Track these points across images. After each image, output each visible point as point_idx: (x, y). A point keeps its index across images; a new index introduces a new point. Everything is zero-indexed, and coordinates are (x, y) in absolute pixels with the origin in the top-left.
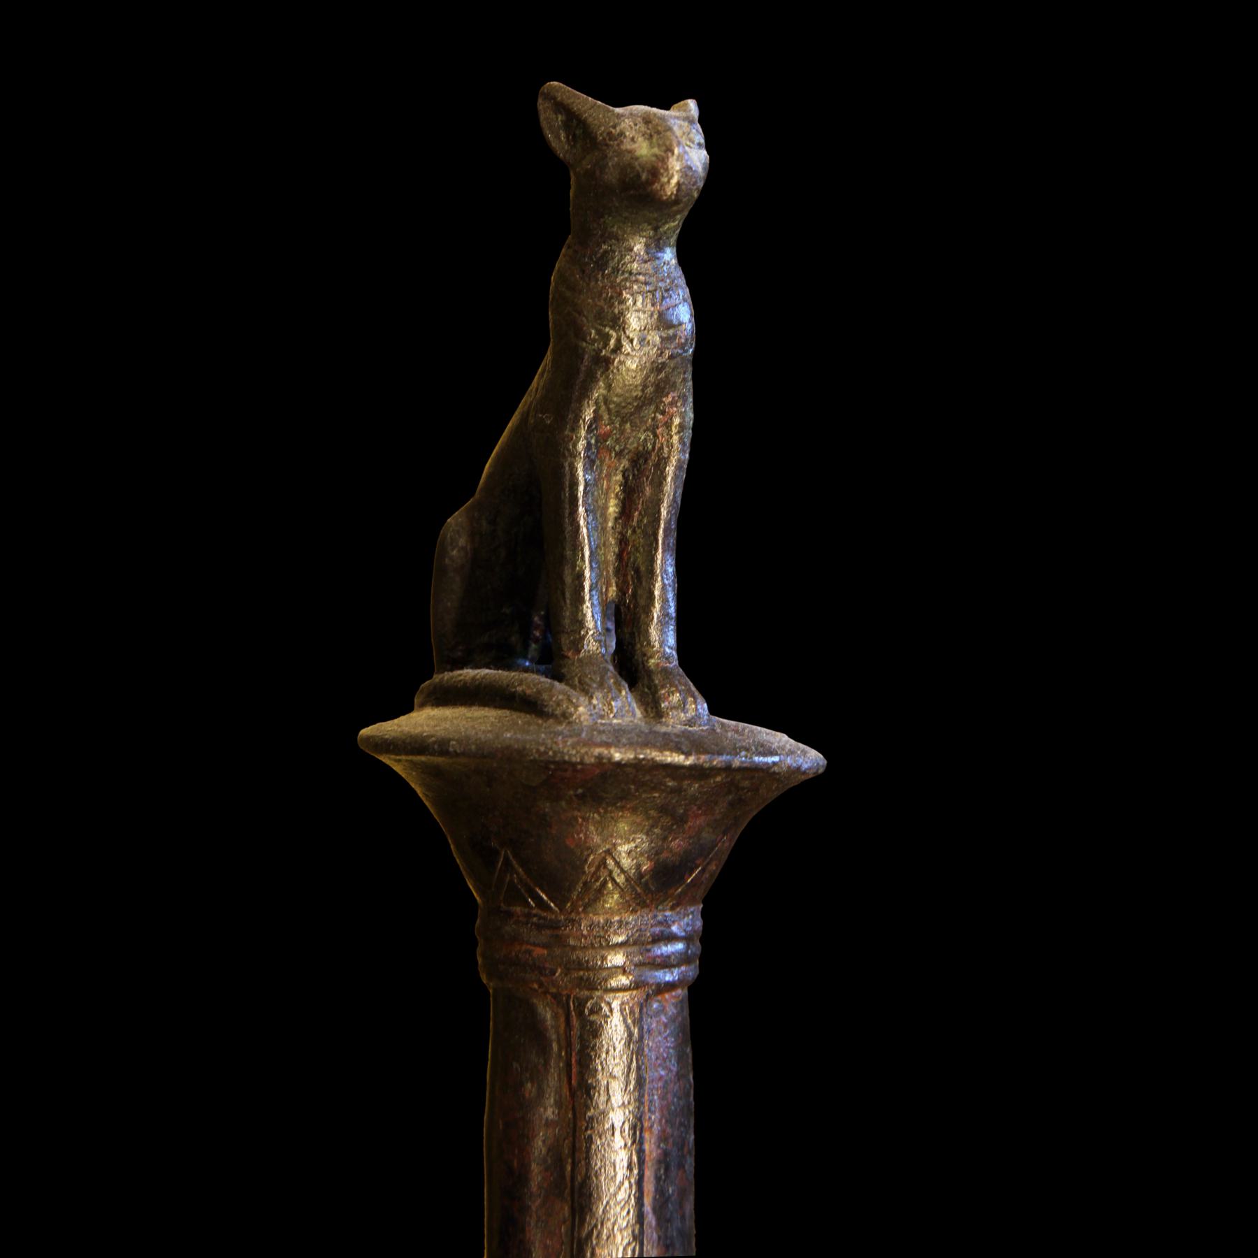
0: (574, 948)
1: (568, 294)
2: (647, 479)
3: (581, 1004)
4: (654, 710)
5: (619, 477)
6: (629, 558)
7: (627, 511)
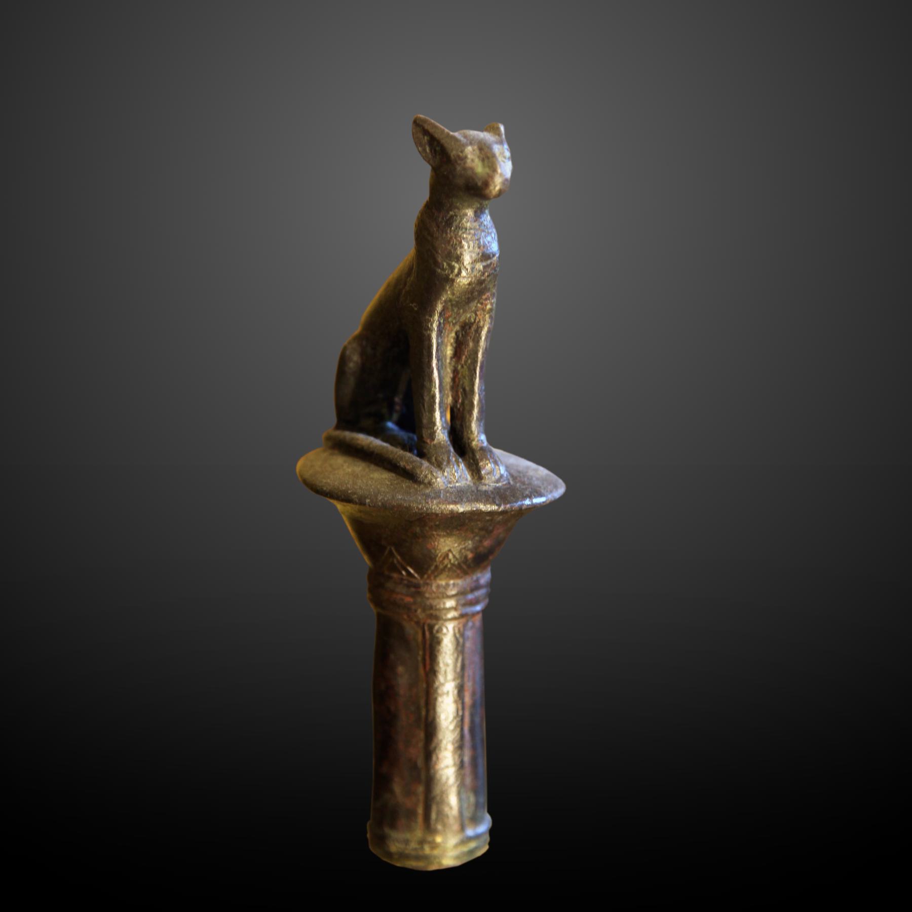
0: (428, 599)
1: (429, 238)
2: (470, 338)
3: (431, 628)
4: (477, 475)
5: (453, 334)
6: (459, 382)
7: (458, 355)
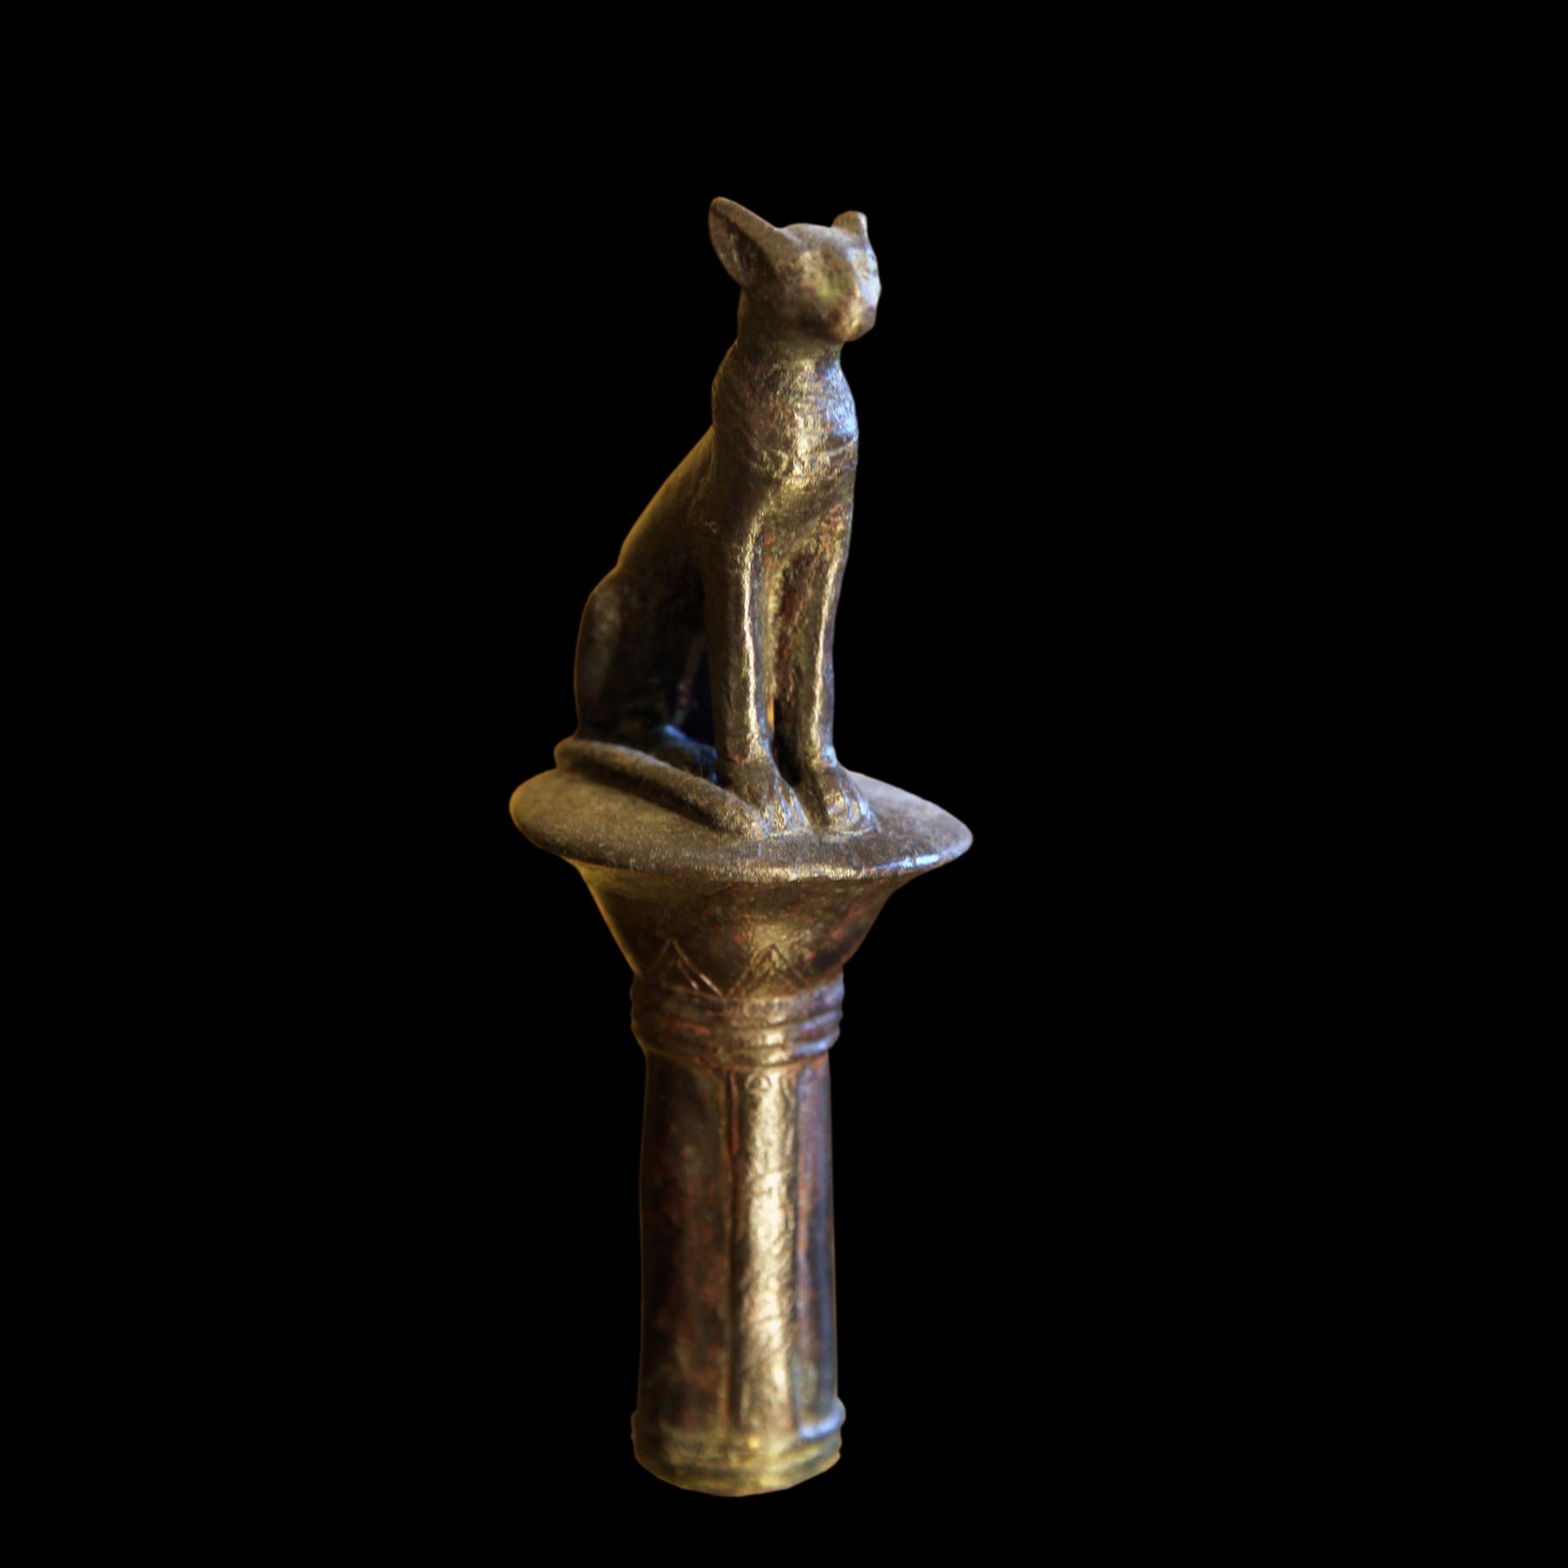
0: (736, 1029)
1: (738, 409)
2: (809, 581)
3: (741, 1079)
4: (821, 816)
5: (779, 575)
6: (789, 657)
7: (788, 610)
